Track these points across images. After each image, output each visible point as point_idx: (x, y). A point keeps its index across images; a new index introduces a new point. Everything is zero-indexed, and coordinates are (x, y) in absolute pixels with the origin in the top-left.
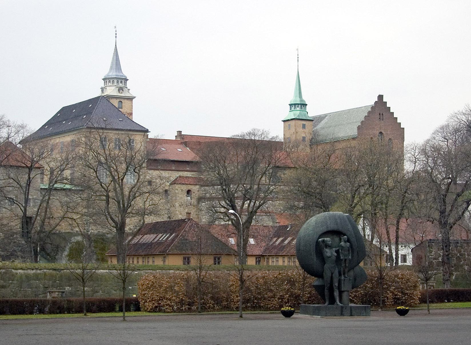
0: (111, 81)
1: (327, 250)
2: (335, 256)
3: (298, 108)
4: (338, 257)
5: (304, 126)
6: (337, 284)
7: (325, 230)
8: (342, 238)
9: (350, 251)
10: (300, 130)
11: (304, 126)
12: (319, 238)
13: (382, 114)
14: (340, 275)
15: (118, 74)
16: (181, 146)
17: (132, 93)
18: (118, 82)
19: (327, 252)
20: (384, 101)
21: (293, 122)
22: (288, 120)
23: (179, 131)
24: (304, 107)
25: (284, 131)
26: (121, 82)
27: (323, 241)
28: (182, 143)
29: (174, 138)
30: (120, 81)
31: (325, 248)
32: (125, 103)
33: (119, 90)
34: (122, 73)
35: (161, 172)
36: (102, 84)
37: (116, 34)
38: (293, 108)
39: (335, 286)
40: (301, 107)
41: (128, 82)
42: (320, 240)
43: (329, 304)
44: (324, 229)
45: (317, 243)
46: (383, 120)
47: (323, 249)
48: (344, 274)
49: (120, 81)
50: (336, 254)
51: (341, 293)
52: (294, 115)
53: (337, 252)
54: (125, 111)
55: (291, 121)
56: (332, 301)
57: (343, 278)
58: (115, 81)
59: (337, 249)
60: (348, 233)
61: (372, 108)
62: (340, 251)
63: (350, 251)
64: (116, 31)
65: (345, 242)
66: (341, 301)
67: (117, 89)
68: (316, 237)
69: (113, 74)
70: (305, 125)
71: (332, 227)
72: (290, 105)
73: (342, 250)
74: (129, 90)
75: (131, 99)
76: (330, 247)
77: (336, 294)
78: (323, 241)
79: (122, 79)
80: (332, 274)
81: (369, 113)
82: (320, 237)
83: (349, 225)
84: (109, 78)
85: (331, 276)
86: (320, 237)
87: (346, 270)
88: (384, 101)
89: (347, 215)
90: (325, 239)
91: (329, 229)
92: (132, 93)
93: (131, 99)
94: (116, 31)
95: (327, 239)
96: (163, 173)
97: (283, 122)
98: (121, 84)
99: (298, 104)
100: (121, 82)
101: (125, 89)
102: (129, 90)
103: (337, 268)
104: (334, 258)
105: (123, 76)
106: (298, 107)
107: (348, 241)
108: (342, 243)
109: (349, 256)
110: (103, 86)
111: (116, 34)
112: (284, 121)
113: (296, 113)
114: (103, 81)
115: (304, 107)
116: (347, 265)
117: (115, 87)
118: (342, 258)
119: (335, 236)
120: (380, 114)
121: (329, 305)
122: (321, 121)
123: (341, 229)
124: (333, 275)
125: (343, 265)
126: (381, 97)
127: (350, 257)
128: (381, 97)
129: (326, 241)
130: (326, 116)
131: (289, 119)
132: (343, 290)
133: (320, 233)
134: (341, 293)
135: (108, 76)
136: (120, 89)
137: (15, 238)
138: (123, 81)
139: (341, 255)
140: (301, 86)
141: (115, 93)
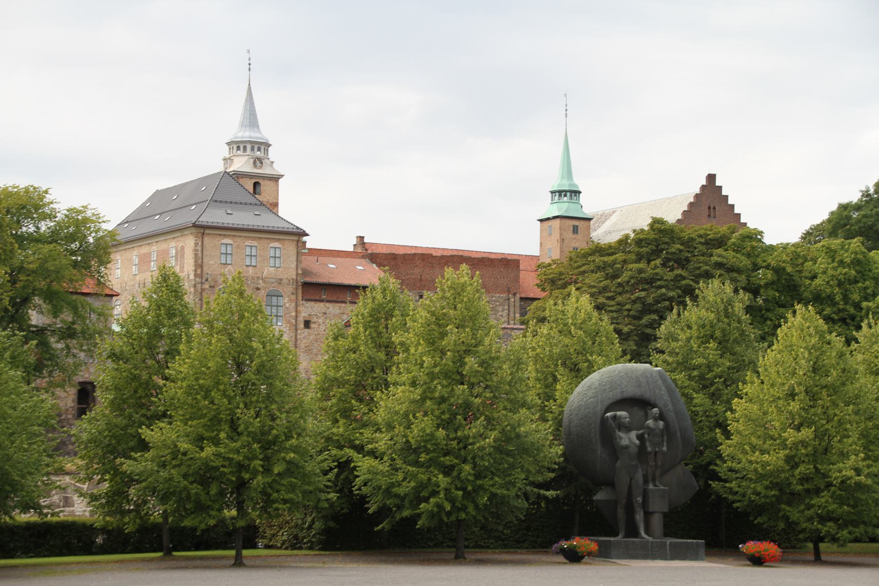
0: (242, 147)
1: (622, 434)
2: (636, 445)
3: (565, 198)
4: (642, 447)
5: (575, 230)
6: (640, 499)
7: (619, 397)
8: (649, 412)
9: (665, 438)
10: (569, 235)
11: (575, 230)
12: (607, 411)
13: (714, 208)
14: (646, 482)
15: (253, 135)
16: (363, 261)
17: (278, 169)
18: (252, 149)
19: (621, 438)
20: (717, 184)
21: (558, 221)
22: (548, 219)
23: (360, 237)
24: (575, 195)
25: (541, 237)
26: (259, 149)
27: (615, 417)
28: (363, 257)
29: (351, 249)
30: (256, 147)
31: (617, 430)
32: (265, 186)
33: (255, 163)
34: (261, 133)
35: (328, 305)
36: (225, 152)
37: (250, 64)
38: (557, 197)
39: (637, 501)
40: (571, 196)
41: (270, 149)
42: (608, 414)
43: (626, 536)
44: (616, 395)
45: (604, 420)
46: (715, 217)
47: (615, 432)
48: (654, 480)
49: (256, 147)
50: (637, 442)
51: (648, 515)
52: (559, 210)
53: (640, 437)
54: (265, 200)
55: (553, 221)
56: (632, 531)
57: (651, 486)
58: (249, 147)
59: (640, 432)
60: (660, 403)
61: (697, 196)
62: (646, 436)
63: (665, 438)
64: (250, 59)
65: (656, 419)
66: (647, 532)
67: (252, 161)
68: (600, 408)
69: (247, 135)
70: (577, 226)
71: (631, 391)
72: (552, 192)
73: (649, 435)
74: (272, 163)
75: (275, 179)
76: (628, 429)
77: (639, 517)
78: (615, 417)
79: (261, 143)
80: (631, 480)
81: (691, 205)
82: (608, 410)
83: (663, 388)
84: (237, 142)
85: (628, 482)
86: (608, 410)
87: (658, 473)
88: (717, 184)
89: (659, 370)
90: (619, 413)
91: (626, 395)
92: (278, 168)
93: (275, 179)
94: (250, 59)
95: (622, 413)
96: (331, 308)
97: (539, 222)
98: (259, 153)
99: (566, 191)
100: (259, 149)
101: (265, 161)
102: (272, 163)
103: (640, 469)
104: (634, 450)
105: (263, 139)
106: (565, 196)
107: (661, 417)
108: (650, 422)
109: (663, 446)
110: (228, 156)
111: (250, 64)
112: (541, 221)
113: (562, 208)
114: (227, 147)
115: (575, 195)
116: (659, 463)
117: (247, 157)
118: (649, 449)
119: (636, 408)
120: (709, 208)
121: (624, 538)
122: (606, 220)
123: (648, 395)
124: (633, 481)
125: (651, 463)
126: (711, 178)
127: (665, 449)
128: (711, 178)
129: (620, 417)
130: (614, 212)
131: (550, 216)
132: (651, 510)
133: (607, 403)
134: (648, 515)
135: (235, 138)
136: (258, 162)
137: (64, 419)
138: (262, 148)
139: (648, 444)
140: (570, 149)
141: (249, 168)
